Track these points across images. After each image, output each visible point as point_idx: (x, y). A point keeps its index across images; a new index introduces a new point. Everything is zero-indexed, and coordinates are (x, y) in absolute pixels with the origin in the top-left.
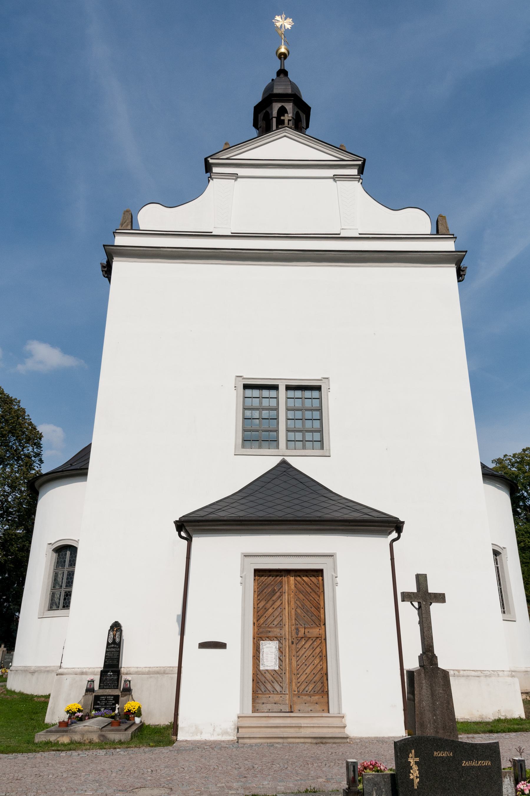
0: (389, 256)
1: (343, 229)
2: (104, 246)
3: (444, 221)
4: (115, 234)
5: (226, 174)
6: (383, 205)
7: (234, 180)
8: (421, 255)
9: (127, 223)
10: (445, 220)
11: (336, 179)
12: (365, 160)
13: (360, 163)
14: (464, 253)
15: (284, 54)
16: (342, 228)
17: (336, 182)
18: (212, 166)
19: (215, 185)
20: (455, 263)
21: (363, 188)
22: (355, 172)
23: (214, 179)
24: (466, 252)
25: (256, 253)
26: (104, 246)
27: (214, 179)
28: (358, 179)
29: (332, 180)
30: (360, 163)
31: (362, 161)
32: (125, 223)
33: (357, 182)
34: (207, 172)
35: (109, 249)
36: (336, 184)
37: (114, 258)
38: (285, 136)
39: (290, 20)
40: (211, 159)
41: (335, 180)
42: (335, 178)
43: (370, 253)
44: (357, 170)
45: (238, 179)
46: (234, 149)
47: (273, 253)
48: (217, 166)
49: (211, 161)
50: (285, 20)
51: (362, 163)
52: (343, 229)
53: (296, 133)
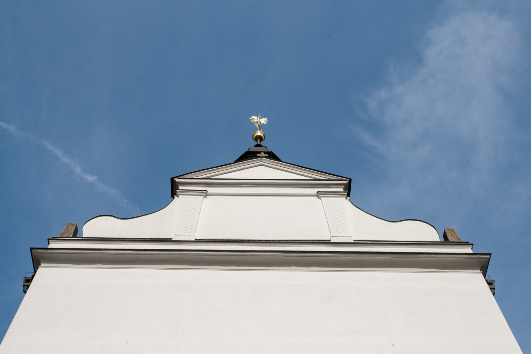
0: (396, 258)
1: (333, 236)
2: (31, 249)
3: (453, 232)
4: (49, 241)
5: (194, 190)
6: (377, 217)
7: (203, 197)
8: (435, 257)
9: (69, 234)
10: (454, 232)
11: (320, 196)
12: (350, 180)
13: (346, 182)
14: (488, 256)
15: (260, 137)
16: (332, 235)
17: (320, 199)
18: (179, 185)
19: (180, 201)
20: (480, 269)
21: (352, 204)
22: (342, 190)
23: (180, 196)
24: (490, 254)
25: (227, 255)
26: (31, 249)
27: (180, 196)
28: (345, 196)
29: (316, 197)
30: (346, 182)
31: (348, 181)
32: (66, 233)
33: (345, 198)
34: (172, 197)
35: (37, 253)
36: (321, 200)
37: (41, 264)
38: (261, 165)
39: (266, 119)
40: (178, 179)
41: (319, 197)
42: (319, 195)
43: (371, 255)
44: (343, 189)
45: (208, 197)
46: (204, 172)
47: (247, 255)
48: (184, 185)
49: (177, 180)
50: (261, 119)
51: (347, 182)
52: (333, 236)
53: (271, 161)
